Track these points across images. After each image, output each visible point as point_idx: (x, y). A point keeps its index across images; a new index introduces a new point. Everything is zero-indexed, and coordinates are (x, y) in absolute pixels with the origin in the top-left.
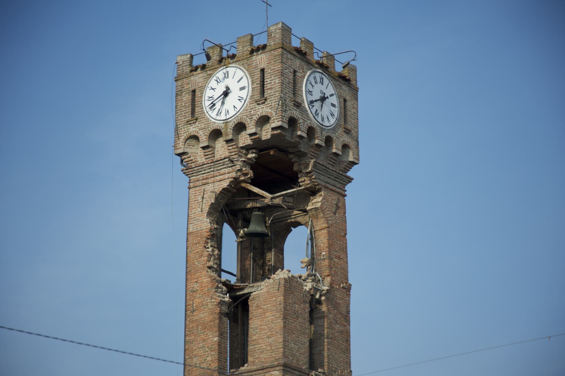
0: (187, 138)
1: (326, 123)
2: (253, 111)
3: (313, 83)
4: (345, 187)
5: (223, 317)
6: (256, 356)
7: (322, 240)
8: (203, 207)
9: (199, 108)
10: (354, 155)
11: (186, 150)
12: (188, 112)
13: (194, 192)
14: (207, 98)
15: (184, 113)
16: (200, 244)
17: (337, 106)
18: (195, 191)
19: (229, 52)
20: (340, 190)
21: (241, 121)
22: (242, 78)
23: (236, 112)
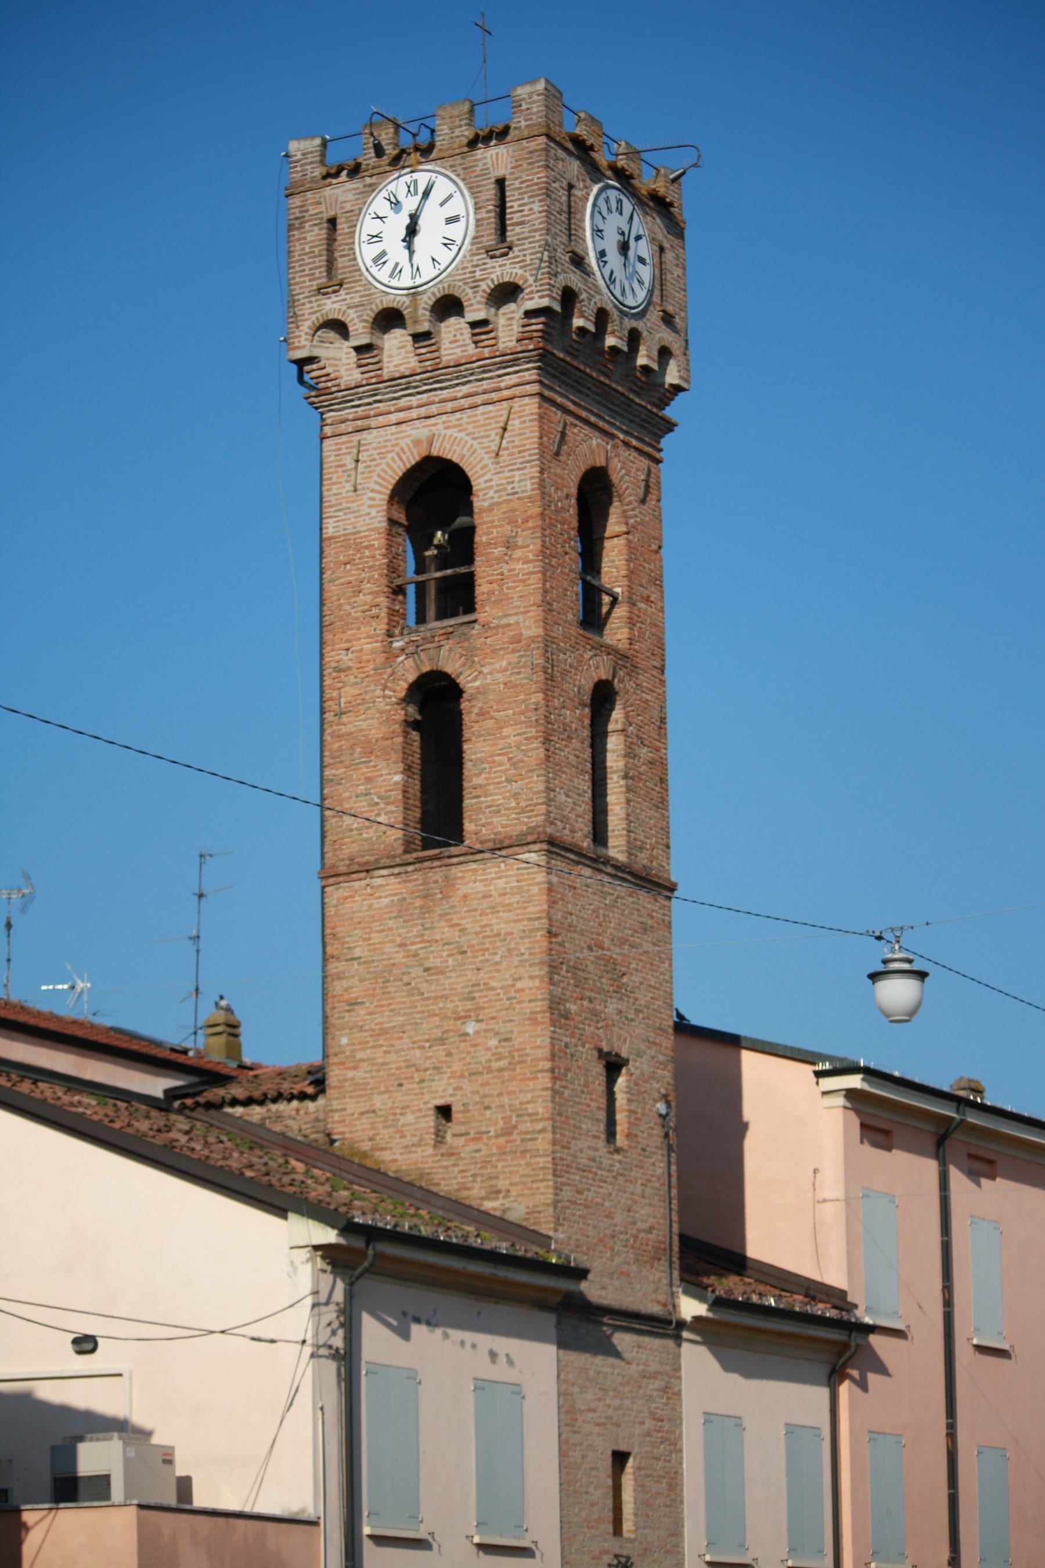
0: (317, 324)
1: (630, 301)
2: (481, 270)
3: (605, 212)
4: (658, 442)
5: (410, 730)
6: (483, 821)
7: (613, 561)
8: (359, 481)
9: (346, 258)
10: (679, 371)
11: (315, 353)
12: (320, 267)
13: (334, 447)
14: (365, 238)
15: (311, 269)
16: (354, 565)
17: (648, 261)
18: (336, 444)
19: (418, 138)
20: (647, 449)
21: (451, 292)
22: (450, 196)
23: (437, 272)
